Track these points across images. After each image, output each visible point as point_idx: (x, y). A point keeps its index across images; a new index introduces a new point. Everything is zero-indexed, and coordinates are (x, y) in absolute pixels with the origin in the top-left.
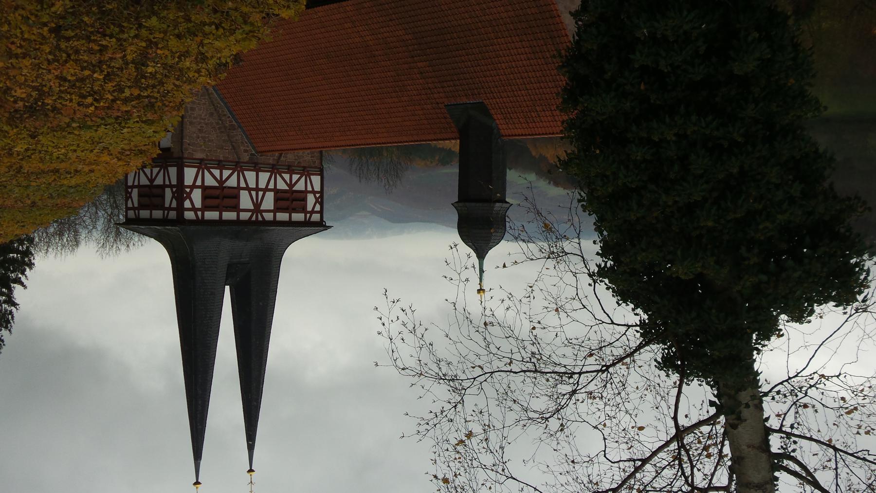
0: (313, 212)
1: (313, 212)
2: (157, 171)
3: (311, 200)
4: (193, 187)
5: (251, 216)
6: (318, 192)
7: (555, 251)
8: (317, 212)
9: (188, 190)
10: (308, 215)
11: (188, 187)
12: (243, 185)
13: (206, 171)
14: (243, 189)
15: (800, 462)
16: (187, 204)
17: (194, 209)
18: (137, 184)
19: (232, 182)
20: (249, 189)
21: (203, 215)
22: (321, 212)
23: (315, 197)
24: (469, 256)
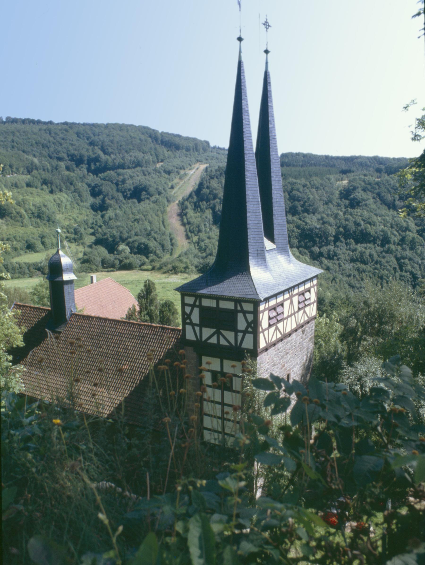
0: (193, 306)
1: (193, 306)
2: (212, 339)
3: (195, 317)
4: (245, 332)
6: (188, 324)
8: (189, 305)
10: (197, 303)
14: (197, 325)
17: (244, 313)
19: (207, 332)
20: (193, 325)
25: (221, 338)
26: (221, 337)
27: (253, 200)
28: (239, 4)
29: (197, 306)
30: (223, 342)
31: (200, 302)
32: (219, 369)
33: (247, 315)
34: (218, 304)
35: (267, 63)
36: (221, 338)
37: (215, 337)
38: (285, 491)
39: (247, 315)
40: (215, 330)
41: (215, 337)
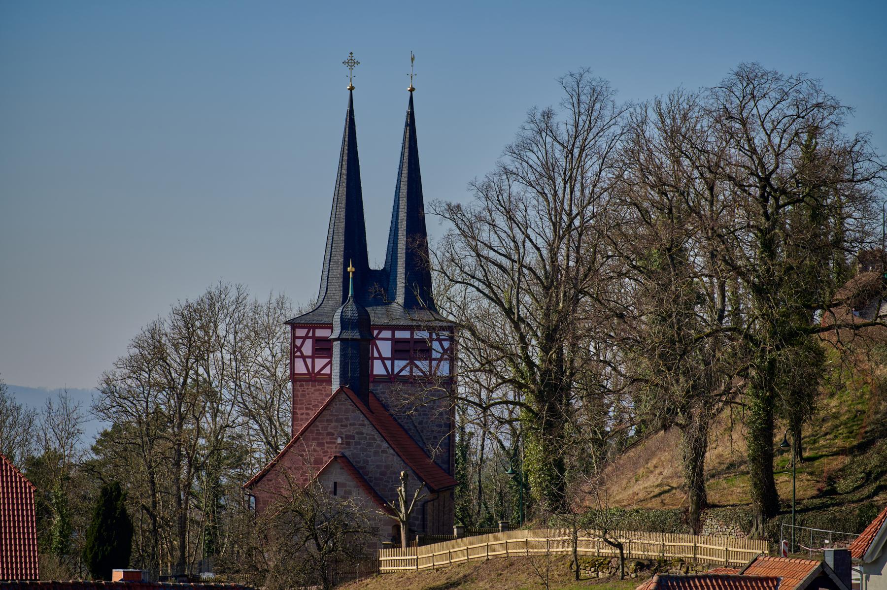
0: (304, 338)
1: (304, 338)
3: (307, 349)
4: (440, 360)
5: (378, 334)
6: (298, 357)
7: (869, 381)
10: (310, 334)
11: (446, 359)
12: (309, 361)
14: (388, 359)
15: (408, 181)
17: (440, 341)
18: (433, 362)
19: (399, 364)
20: (304, 357)
22: (294, 337)
23: (301, 352)
25: (415, 369)
28: (413, 59)
30: (417, 373)
31: (314, 333)
34: (412, 334)
36: (415, 369)
37: (408, 369)
40: (408, 361)
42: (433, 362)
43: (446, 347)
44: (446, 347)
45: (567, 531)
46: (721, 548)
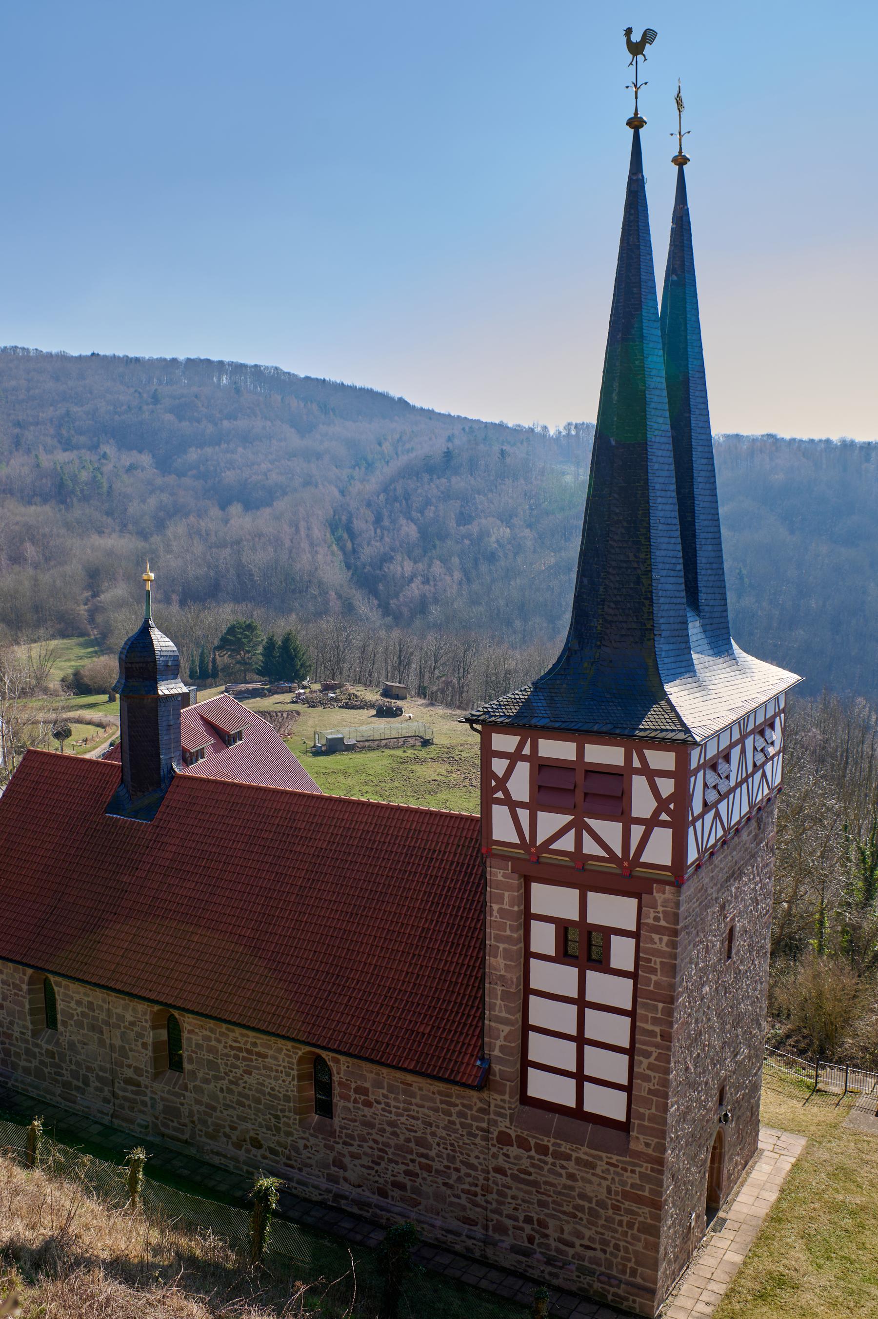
0: (514, 758)
1: (514, 758)
4: (651, 824)
6: (499, 802)
8: (502, 755)
9: (664, 817)
10: (526, 751)
11: (664, 824)
13: (619, 853)
14: (523, 805)
16: (666, 787)
17: (651, 775)
18: (634, 827)
20: (513, 805)
21: (628, 759)
22: (487, 753)
23: (506, 793)
24: (561, 642)
25: (586, 836)
26: (585, 835)
27: (663, 493)
29: (525, 758)
30: (590, 847)
31: (535, 748)
32: (576, 917)
33: (659, 781)
35: (636, 98)
37: (571, 834)
38: (669, 1228)
39: (659, 781)
41: (571, 834)
42: (634, 827)
43: (664, 795)
44: (664, 795)
45: (799, 1094)
46: (513, 1045)
